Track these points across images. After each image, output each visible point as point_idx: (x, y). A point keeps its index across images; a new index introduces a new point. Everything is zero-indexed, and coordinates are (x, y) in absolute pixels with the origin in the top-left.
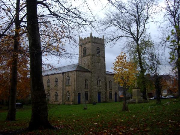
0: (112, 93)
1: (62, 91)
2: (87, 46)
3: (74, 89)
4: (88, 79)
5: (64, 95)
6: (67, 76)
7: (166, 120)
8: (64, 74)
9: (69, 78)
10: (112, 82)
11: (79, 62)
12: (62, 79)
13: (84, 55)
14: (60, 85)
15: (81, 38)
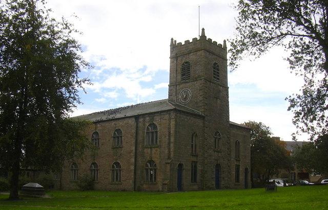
1: (133, 160)
2: (192, 58)
8: (141, 120)
10: (241, 144)
11: (170, 95)
12: (134, 131)
13: (183, 79)
14: (128, 145)
15: (175, 41)
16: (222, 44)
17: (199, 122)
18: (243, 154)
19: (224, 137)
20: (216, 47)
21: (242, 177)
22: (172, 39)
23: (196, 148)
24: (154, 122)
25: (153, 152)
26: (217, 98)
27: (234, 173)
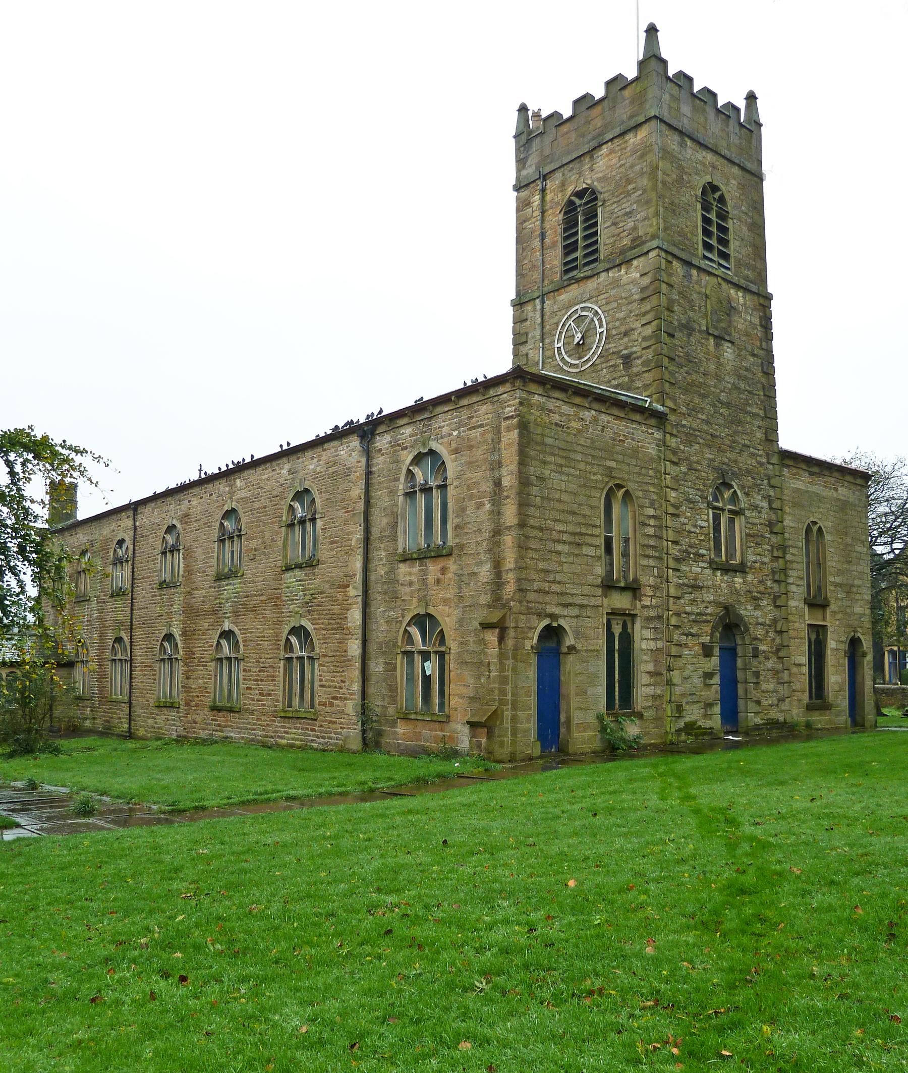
0: (831, 644)
1: (355, 616)
2: (602, 169)
3: (498, 582)
4: (631, 486)
5: (373, 648)
6: (407, 457)
7: (738, 762)
9: (440, 467)
10: (828, 537)
13: (569, 267)
16: (741, 104)
17: (645, 439)
18: (838, 580)
19: (756, 508)
20: (711, 114)
21: (836, 677)
22: (523, 109)
23: (625, 554)
24: (434, 445)
25: (431, 578)
26: (719, 338)
27: (804, 660)
